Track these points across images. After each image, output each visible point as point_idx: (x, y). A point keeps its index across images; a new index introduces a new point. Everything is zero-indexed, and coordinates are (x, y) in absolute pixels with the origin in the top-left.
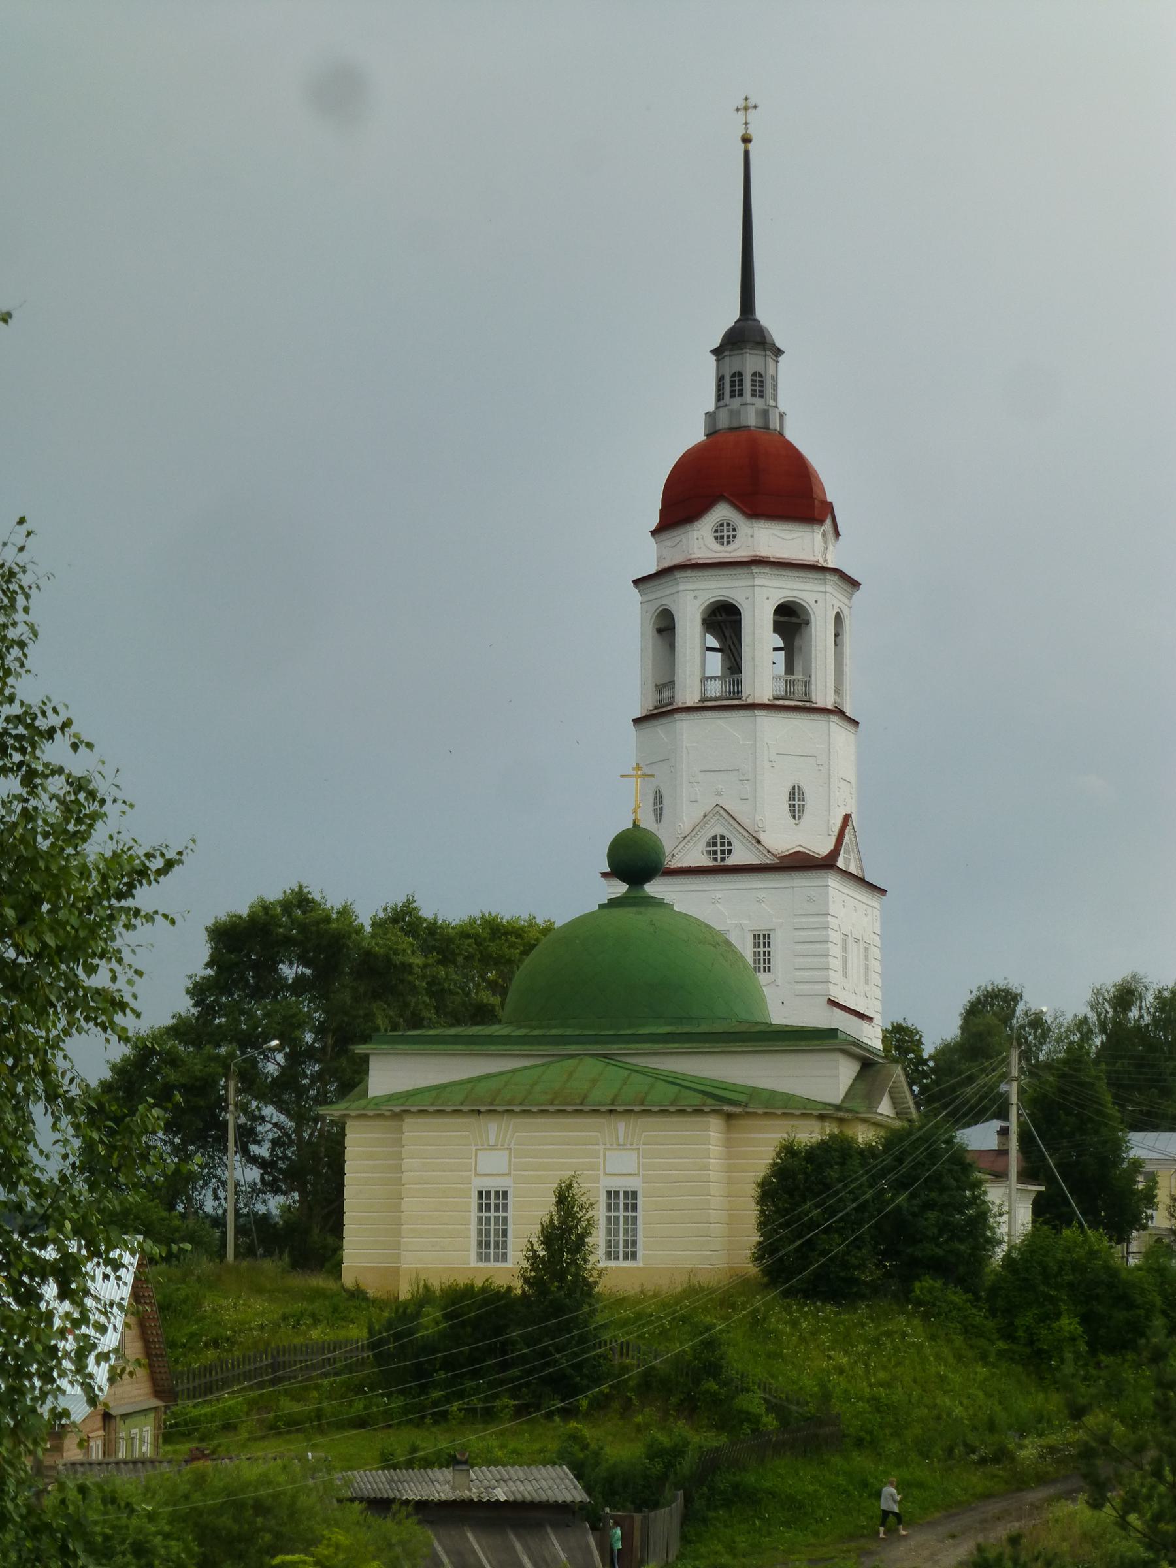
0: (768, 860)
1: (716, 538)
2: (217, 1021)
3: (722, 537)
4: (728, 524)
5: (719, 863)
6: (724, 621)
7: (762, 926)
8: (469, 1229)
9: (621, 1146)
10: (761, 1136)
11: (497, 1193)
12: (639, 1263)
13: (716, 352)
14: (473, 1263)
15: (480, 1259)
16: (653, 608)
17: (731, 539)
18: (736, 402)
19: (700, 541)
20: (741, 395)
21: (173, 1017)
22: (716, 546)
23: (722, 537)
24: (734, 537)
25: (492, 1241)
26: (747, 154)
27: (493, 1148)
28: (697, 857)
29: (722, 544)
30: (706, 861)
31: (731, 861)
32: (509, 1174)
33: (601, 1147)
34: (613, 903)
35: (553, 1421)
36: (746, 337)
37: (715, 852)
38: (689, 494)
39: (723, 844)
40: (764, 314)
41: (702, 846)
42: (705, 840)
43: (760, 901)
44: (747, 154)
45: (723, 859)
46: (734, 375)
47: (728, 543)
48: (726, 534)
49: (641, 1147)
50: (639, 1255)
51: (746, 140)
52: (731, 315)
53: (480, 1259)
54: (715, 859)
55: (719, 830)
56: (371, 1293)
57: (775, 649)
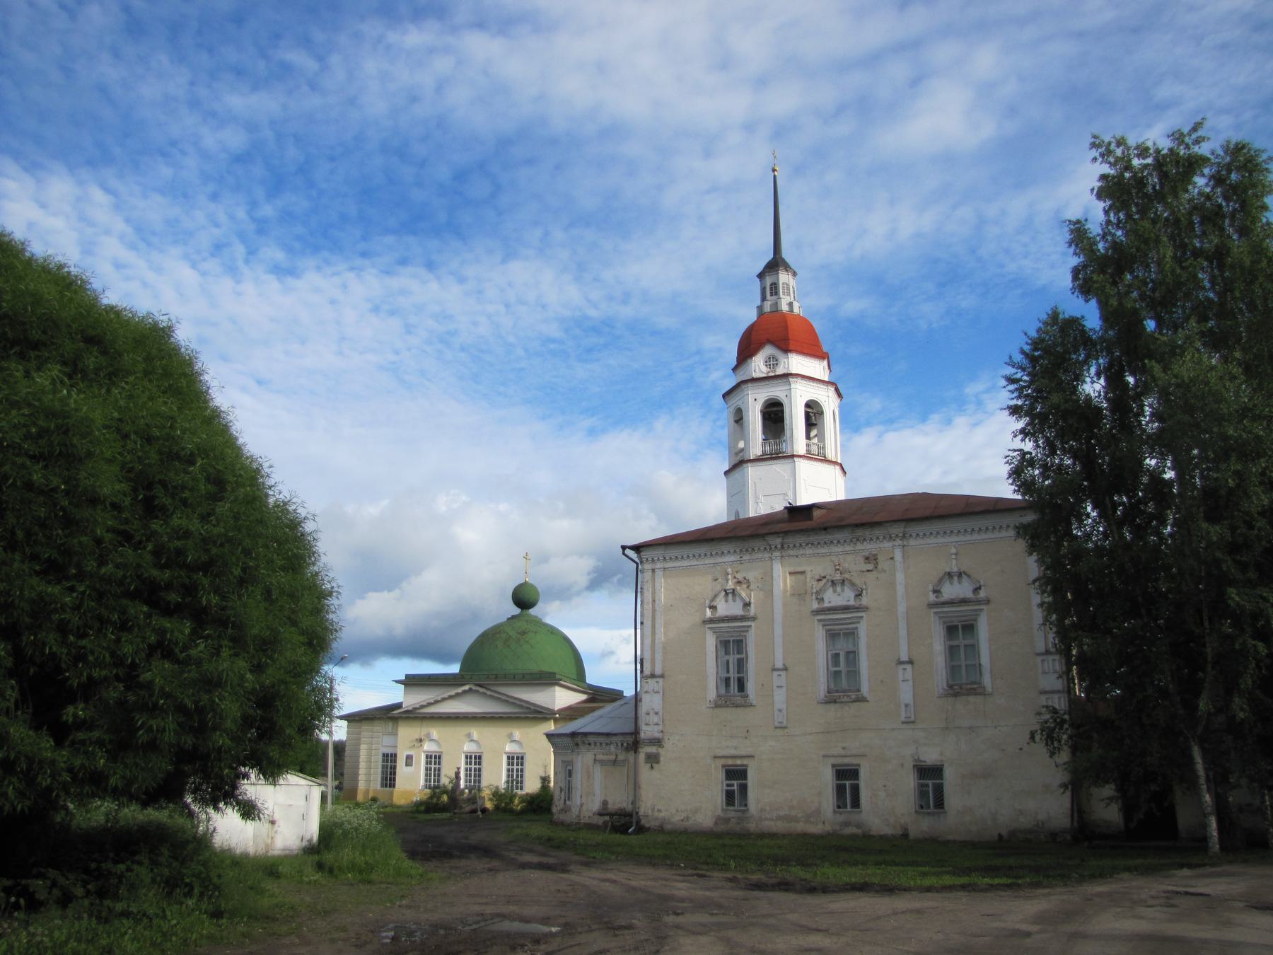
16: (732, 409)
19: (758, 365)
36: (776, 264)
51: (774, 170)
57: (736, 774)
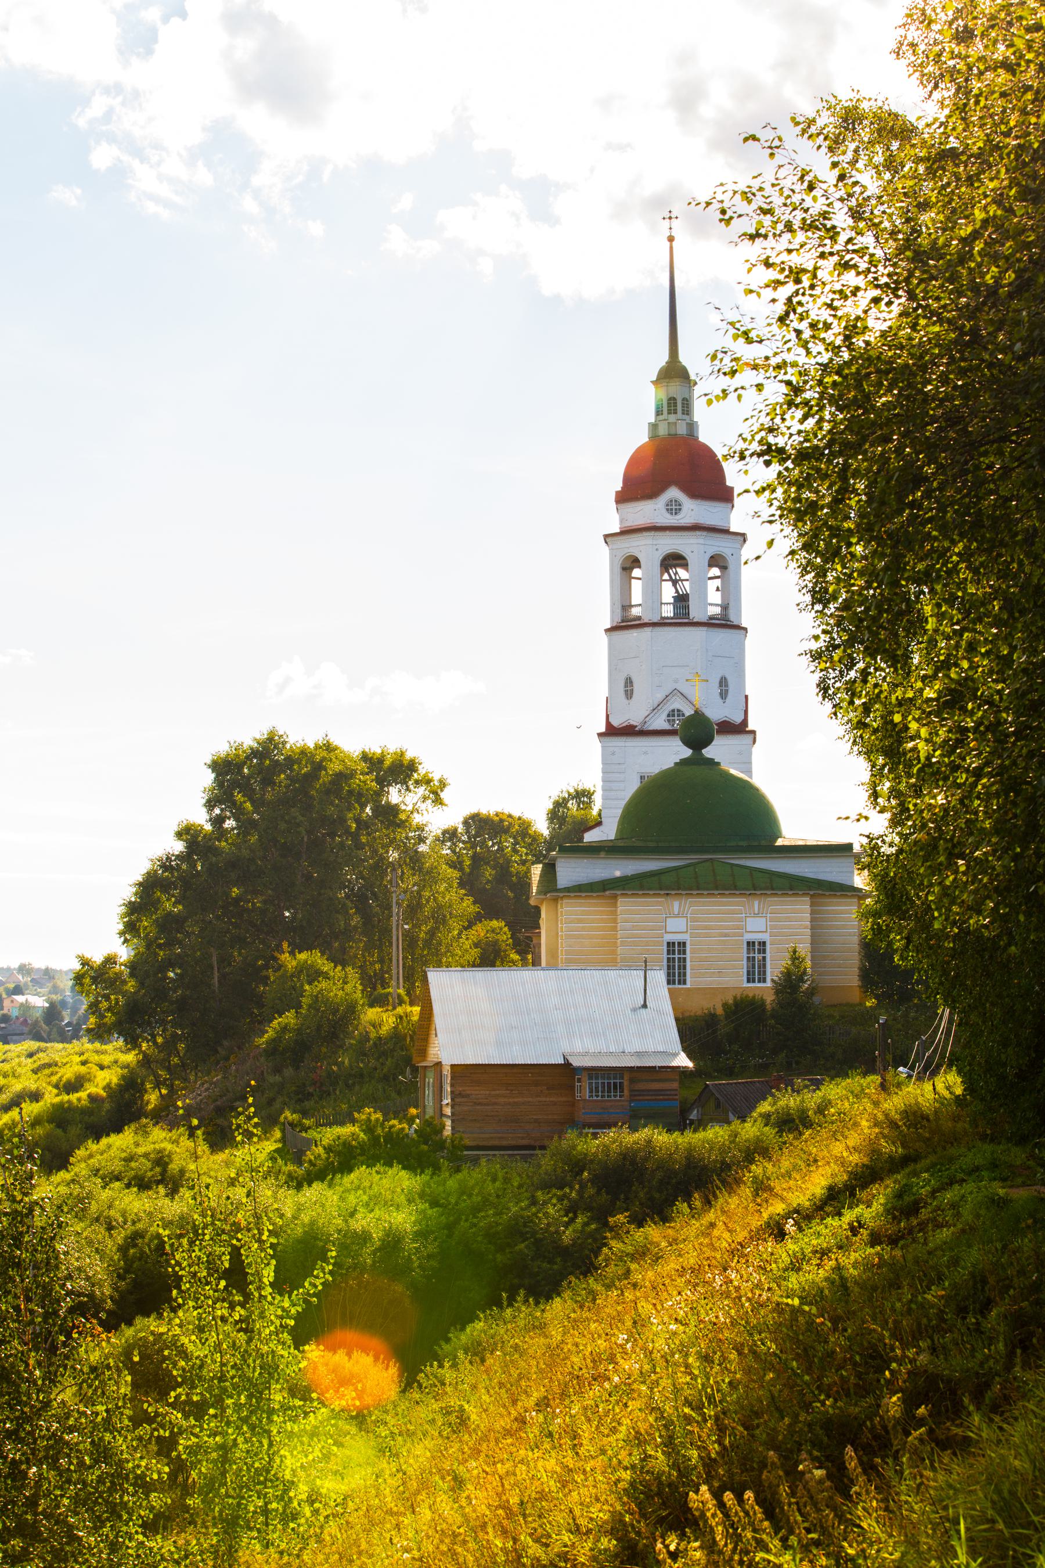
2: (961, 862)
9: (756, 915)
12: (688, 986)
14: (746, 985)
15: (748, 981)
17: (677, 511)
18: (672, 418)
20: (675, 413)
21: (179, 835)
22: (668, 516)
25: (756, 971)
27: (677, 916)
30: (666, 726)
34: (684, 762)
35: (104, 1089)
38: (637, 486)
41: (664, 716)
48: (674, 508)
51: (671, 239)
52: (664, 358)
53: (748, 981)
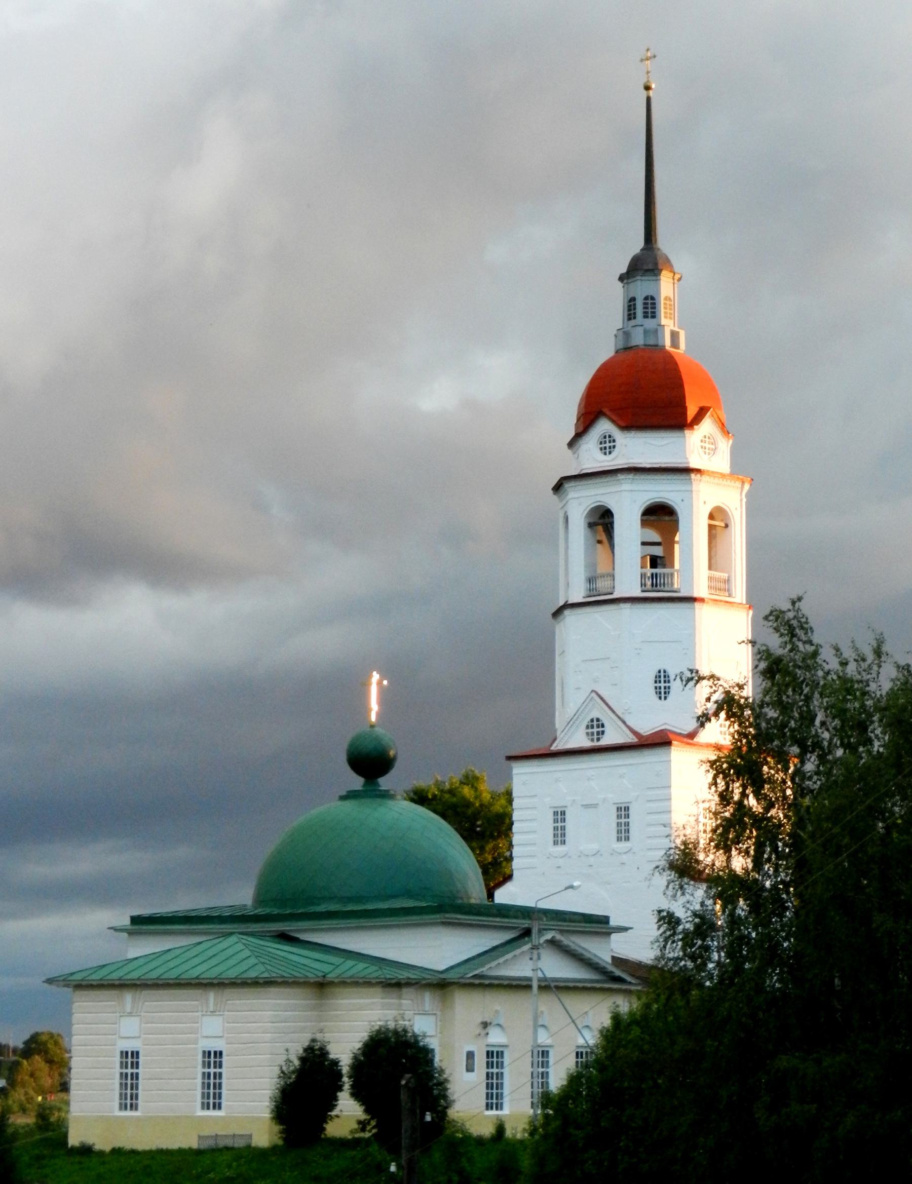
0: (631, 739)
1: (601, 449)
3: (605, 448)
4: (610, 436)
5: (596, 744)
6: (602, 521)
7: (623, 799)
8: (113, 1084)
10: (358, 1001)
11: (215, 1053)
13: (621, 278)
22: (601, 457)
23: (605, 448)
24: (614, 447)
26: (649, 100)
28: (580, 740)
29: (605, 454)
30: (587, 744)
31: (606, 741)
32: (139, 1037)
33: (199, 1014)
37: (593, 734)
39: (592, 727)
40: (664, 243)
42: (586, 722)
43: (621, 776)
44: (649, 100)
45: (598, 740)
46: (646, 298)
47: (610, 453)
49: (143, 1014)
50: (223, 1106)
52: (638, 244)
53: (121, 1109)
54: (592, 740)
55: (595, 714)
56: (97, 1147)
